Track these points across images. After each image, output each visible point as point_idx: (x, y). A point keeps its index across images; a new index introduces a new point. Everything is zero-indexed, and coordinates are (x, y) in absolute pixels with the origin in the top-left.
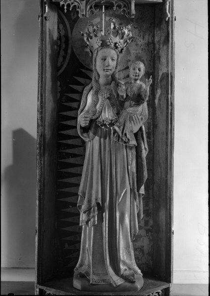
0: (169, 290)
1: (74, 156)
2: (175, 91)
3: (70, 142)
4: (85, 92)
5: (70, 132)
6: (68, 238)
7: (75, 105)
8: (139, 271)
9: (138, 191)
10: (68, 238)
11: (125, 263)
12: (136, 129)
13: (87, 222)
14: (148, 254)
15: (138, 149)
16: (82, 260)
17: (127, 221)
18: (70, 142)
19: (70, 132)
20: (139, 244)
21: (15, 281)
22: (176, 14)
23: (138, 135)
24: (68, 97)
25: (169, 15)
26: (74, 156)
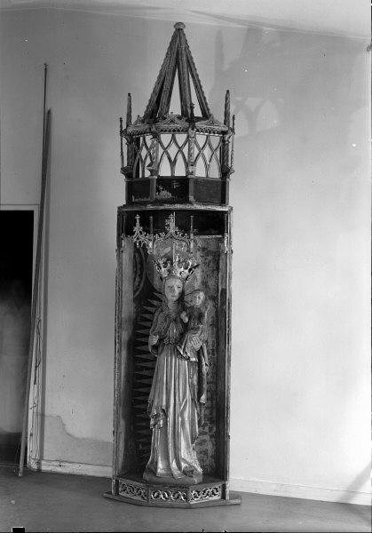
0: (124, 467)
1: (147, 369)
2: (232, 394)
3: (144, 356)
4: (156, 314)
5: (143, 348)
6: (141, 440)
7: (148, 324)
8: (200, 470)
9: (199, 401)
10: (141, 440)
11: (186, 462)
12: (197, 347)
13: (154, 425)
14: (212, 457)
15: (199, 363)
16: (153, 459)
17: (187, 426)
18: (144, 356)
19: (143, 348)
20: (204, 448)
21: (326, 500)
22: (234, 247)
23: (199, 353)
24: (142, 317)
25: (227, 249)
26: (147, 369)
